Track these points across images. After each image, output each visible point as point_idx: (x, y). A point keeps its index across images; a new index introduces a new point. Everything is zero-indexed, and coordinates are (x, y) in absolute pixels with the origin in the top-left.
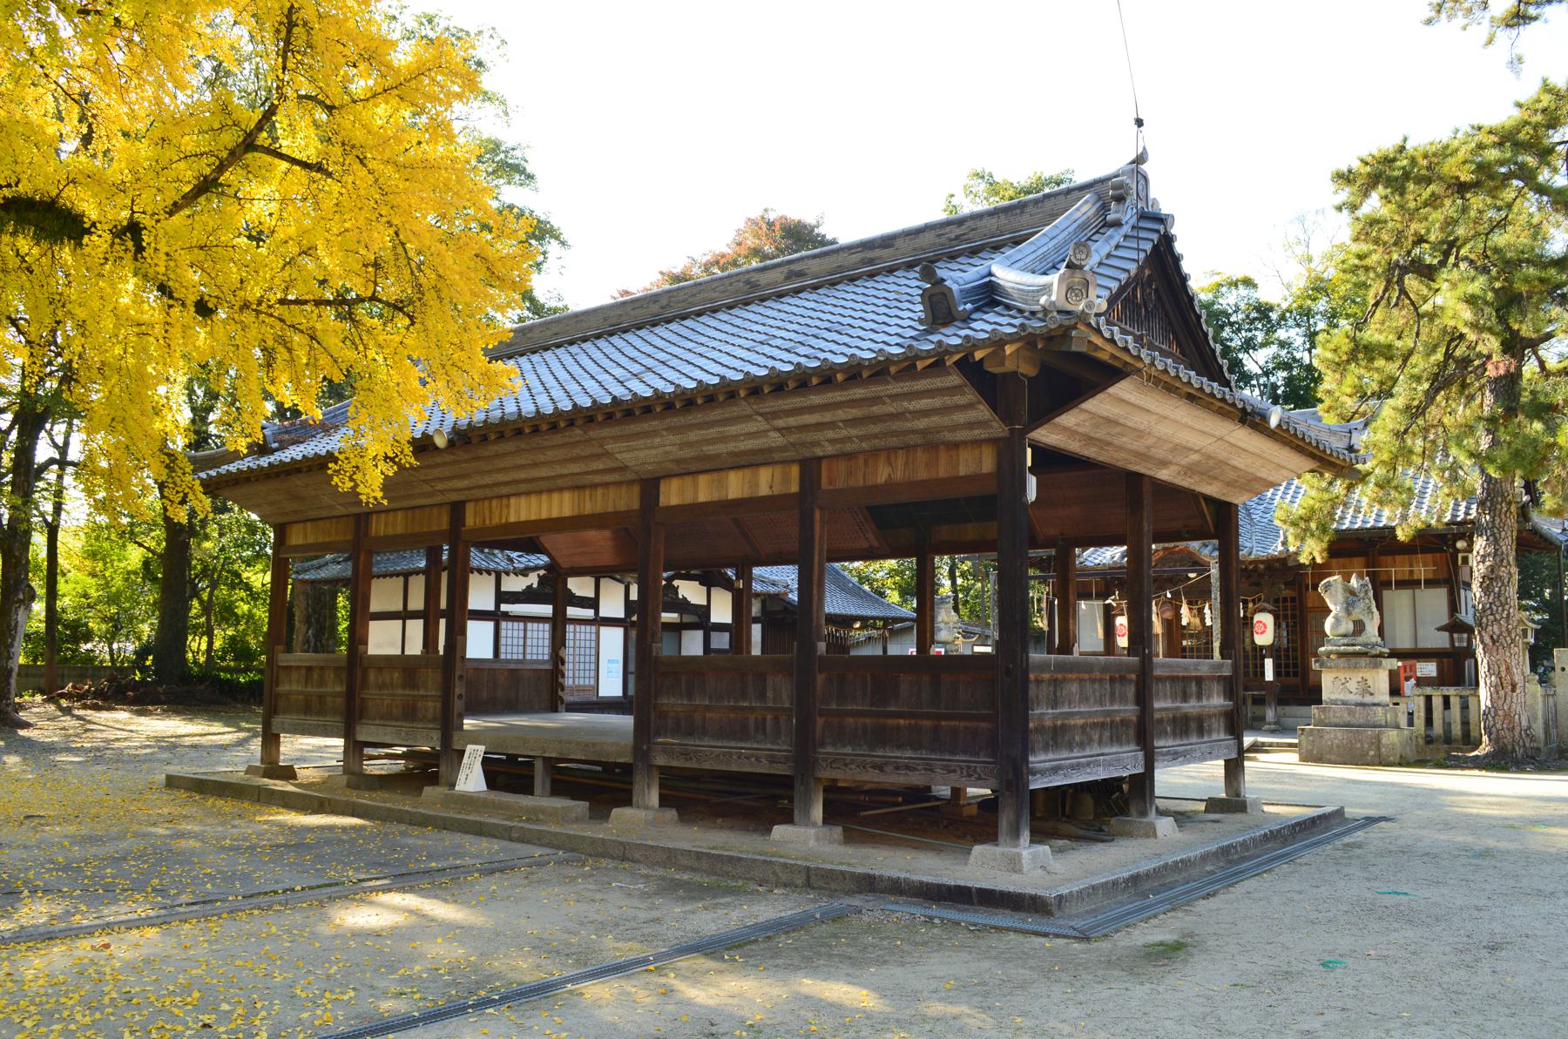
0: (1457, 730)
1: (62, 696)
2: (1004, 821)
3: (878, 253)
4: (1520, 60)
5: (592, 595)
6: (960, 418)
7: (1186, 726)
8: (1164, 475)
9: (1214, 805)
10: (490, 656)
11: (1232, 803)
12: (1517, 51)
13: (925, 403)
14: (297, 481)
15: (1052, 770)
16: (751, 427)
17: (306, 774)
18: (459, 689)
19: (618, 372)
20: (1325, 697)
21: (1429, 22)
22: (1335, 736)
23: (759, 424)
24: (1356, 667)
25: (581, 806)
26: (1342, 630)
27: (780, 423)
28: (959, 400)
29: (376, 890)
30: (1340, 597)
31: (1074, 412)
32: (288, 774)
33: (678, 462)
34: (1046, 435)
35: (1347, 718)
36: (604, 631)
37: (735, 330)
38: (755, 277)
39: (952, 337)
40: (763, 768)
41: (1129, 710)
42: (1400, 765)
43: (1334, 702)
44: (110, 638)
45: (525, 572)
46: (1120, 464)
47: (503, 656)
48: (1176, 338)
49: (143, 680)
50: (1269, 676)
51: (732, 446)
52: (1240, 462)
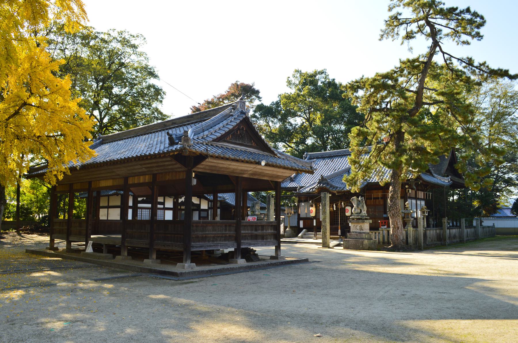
0: (381, 239)
1: (21, 230)
2: (184, 257)
3: (190, 119)
4: (411, 48)
5: (163, 201)
8: (245, 176)
9: (272, 258)
12: (409, 47)
15: (197, 247)
17: (61, 249)
21: (380, 40)
22: (352, 241)
23: (139, 167)
24: (358, 223)
26: (356, 212)
29: (45, 271)
30: (356, 203)
32: (57, 249)
35: (356, 237)
36: (166, 212)
38: (166, 124)
40: (144, 246)
41: (233, 233)
42: (368, 250)
43: (353, 232)
47: (139, 218)
49: (44, 225)
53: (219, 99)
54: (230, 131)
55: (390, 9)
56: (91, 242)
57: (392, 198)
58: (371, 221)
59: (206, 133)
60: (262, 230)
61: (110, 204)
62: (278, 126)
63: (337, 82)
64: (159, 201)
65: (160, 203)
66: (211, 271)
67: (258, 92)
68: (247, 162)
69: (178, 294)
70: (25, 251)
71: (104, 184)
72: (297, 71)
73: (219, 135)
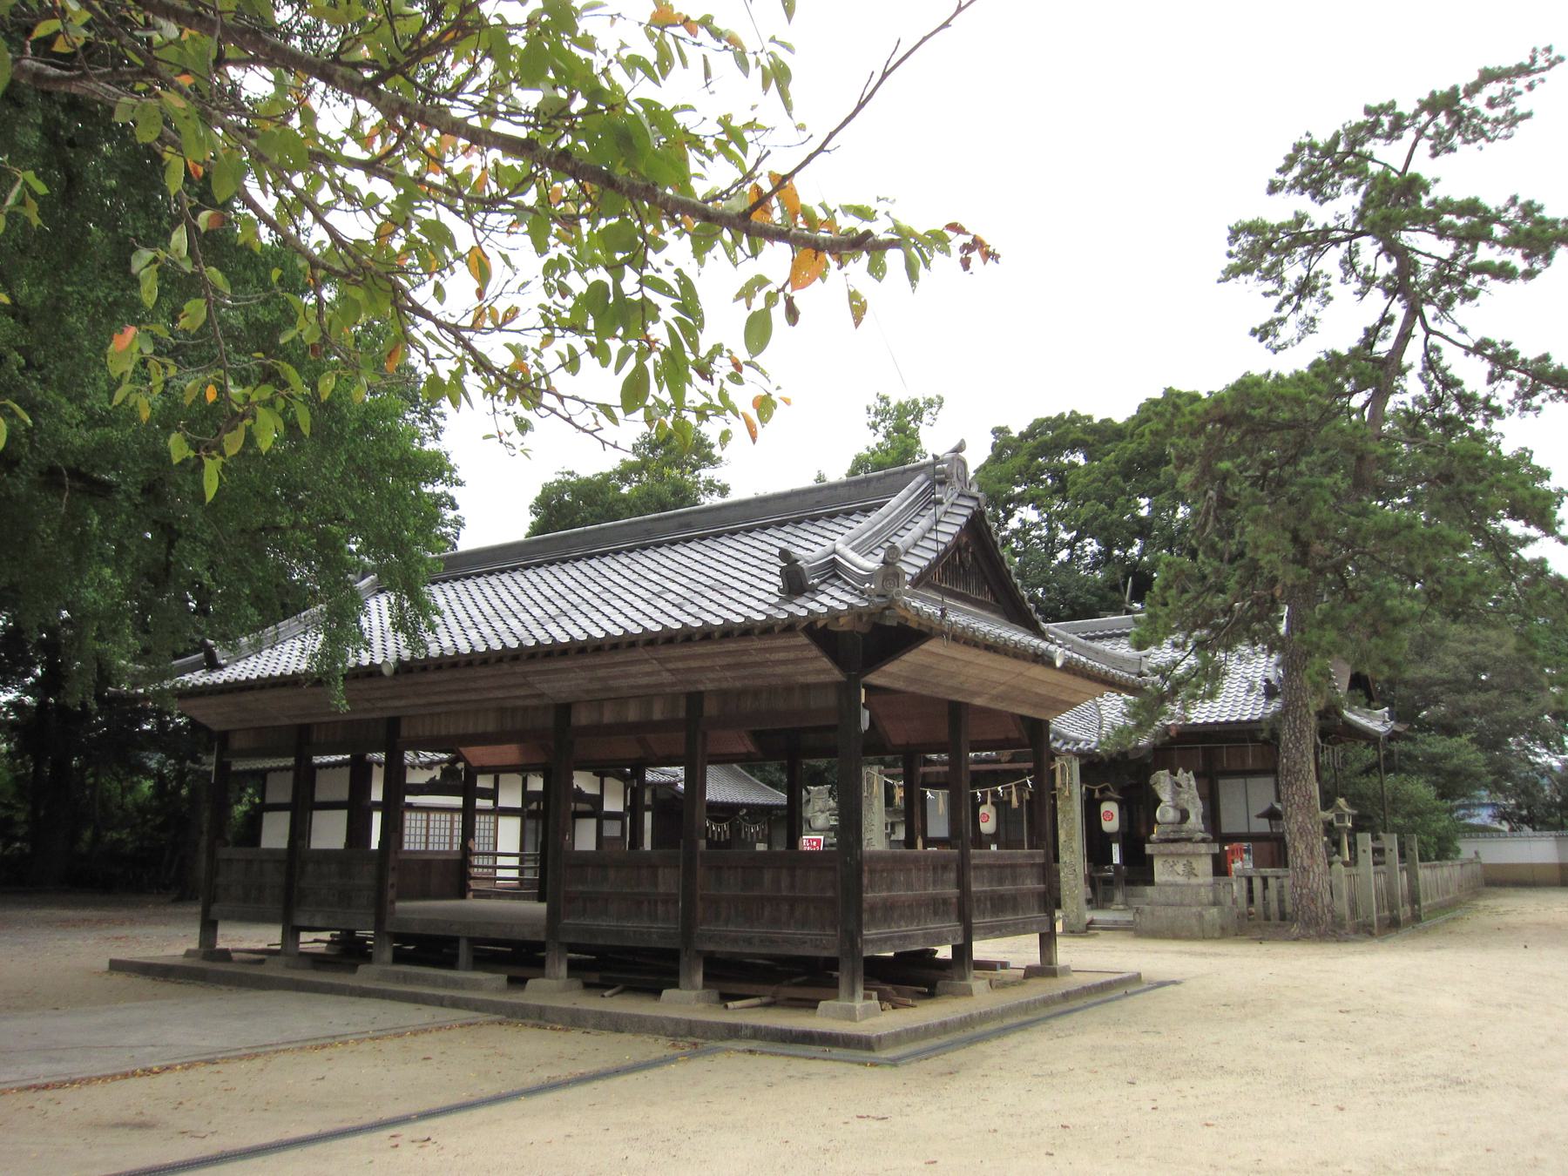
0: (1274, 906)
6: (810, 666)
7: (1000, 904)
11: (1045, 969)
13: (782, 656)
14: (248, 697)
16: (647, 668)
18: (392, 879)
19: (537, 612)
20: (1156, 879)
25: (502, 979)
27: (671, 666)
28: (810, 655)
30: (1168, 788)
31: (896, 662)
33: (588, 692)
34: (874, 679)
37: (634, 577)
39: (801, 608)
41: (952, 892)
45: (430, 765)
46: (940, 695)
48: (991, 589)
50: (1116, 859)
51: (632, 681)
52: (1042, 690)
60: (1014, 880)
64: (479, 785)
70: (106, 965)
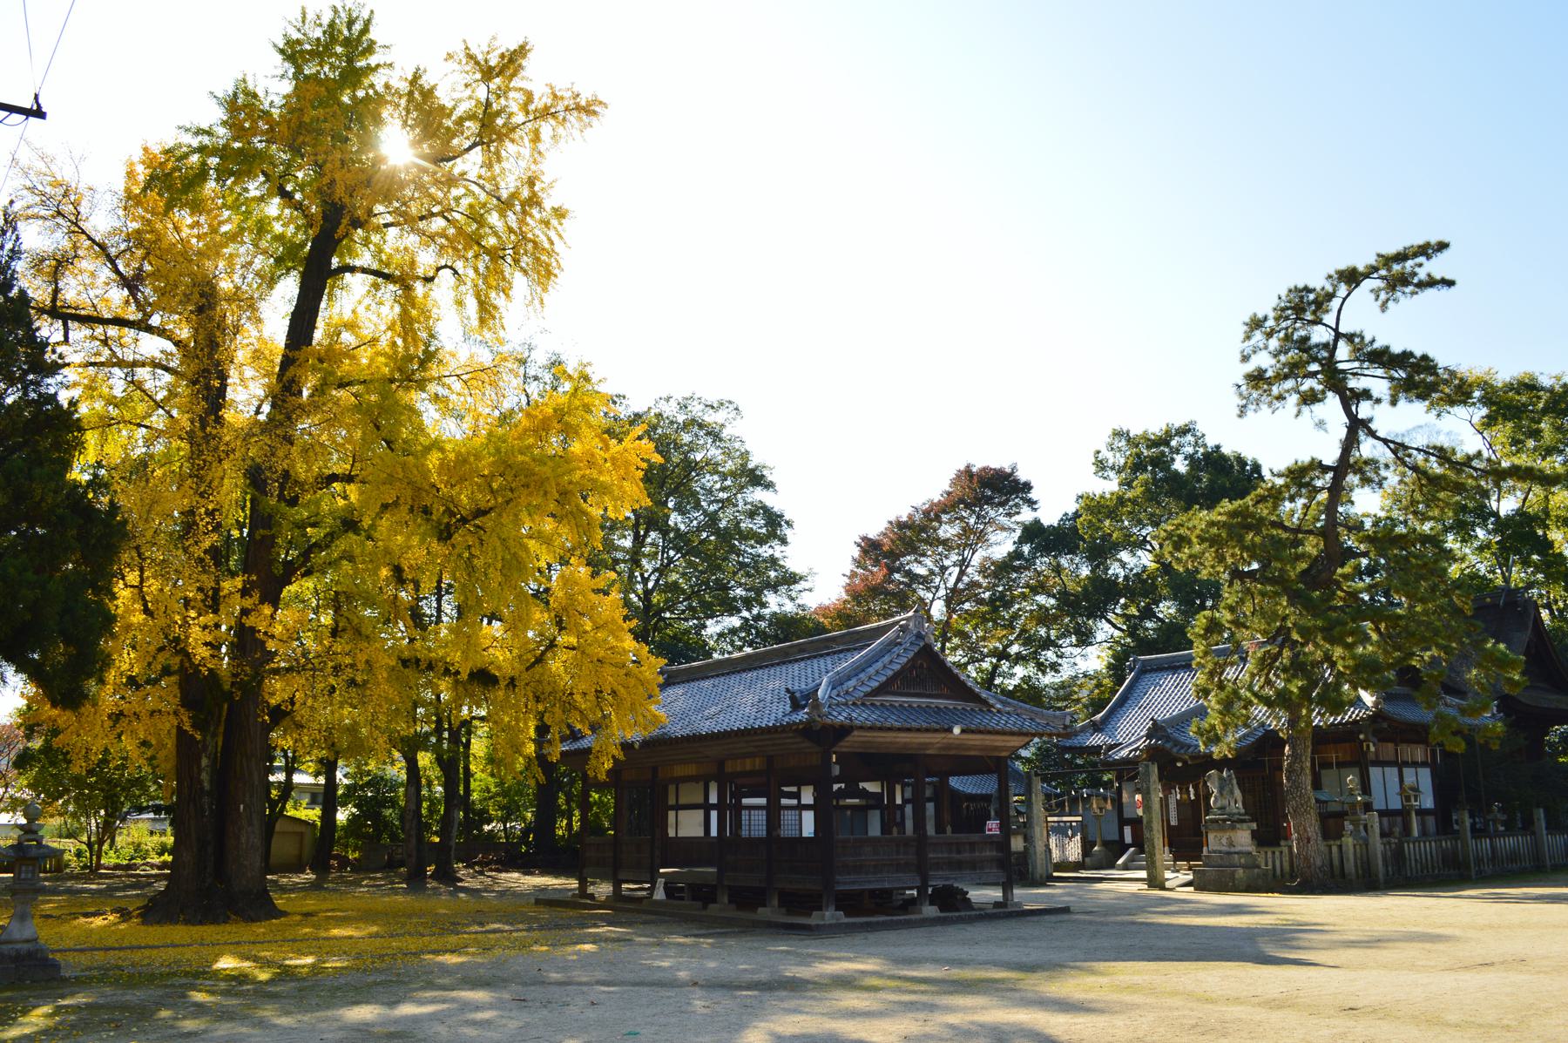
10: (701, 834)
15: (847, 883)
32: (592, 897)
44: (504, 820)
47: (745, 833)
53: (926, 513)
54: (897, 675)
55: (1245, 359)
56: (661, 881)
57: (1290, 771)
58: (1254, 826)
59: (853, 682)
60: (972, 851)
61: (682, 801)
62: (1085, 571)
63: (1226, 450)
65: (790, 795)
66: (868, 924)
67: (1027, 487)
68: (927, 730)
69: (808, 947)
71: (680, 771)
72: (1118, 434)
73: (875, 684)
